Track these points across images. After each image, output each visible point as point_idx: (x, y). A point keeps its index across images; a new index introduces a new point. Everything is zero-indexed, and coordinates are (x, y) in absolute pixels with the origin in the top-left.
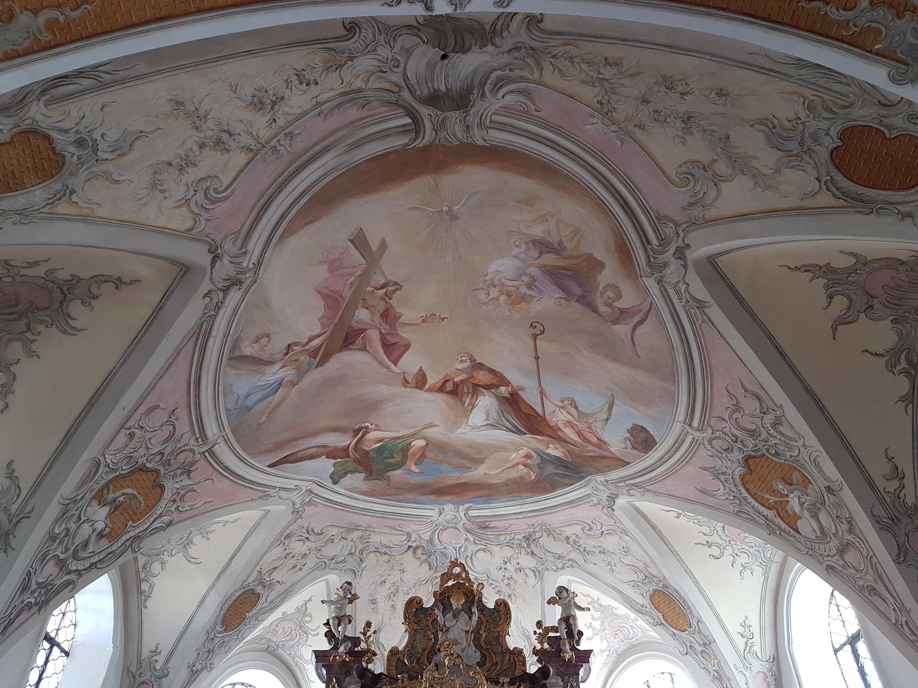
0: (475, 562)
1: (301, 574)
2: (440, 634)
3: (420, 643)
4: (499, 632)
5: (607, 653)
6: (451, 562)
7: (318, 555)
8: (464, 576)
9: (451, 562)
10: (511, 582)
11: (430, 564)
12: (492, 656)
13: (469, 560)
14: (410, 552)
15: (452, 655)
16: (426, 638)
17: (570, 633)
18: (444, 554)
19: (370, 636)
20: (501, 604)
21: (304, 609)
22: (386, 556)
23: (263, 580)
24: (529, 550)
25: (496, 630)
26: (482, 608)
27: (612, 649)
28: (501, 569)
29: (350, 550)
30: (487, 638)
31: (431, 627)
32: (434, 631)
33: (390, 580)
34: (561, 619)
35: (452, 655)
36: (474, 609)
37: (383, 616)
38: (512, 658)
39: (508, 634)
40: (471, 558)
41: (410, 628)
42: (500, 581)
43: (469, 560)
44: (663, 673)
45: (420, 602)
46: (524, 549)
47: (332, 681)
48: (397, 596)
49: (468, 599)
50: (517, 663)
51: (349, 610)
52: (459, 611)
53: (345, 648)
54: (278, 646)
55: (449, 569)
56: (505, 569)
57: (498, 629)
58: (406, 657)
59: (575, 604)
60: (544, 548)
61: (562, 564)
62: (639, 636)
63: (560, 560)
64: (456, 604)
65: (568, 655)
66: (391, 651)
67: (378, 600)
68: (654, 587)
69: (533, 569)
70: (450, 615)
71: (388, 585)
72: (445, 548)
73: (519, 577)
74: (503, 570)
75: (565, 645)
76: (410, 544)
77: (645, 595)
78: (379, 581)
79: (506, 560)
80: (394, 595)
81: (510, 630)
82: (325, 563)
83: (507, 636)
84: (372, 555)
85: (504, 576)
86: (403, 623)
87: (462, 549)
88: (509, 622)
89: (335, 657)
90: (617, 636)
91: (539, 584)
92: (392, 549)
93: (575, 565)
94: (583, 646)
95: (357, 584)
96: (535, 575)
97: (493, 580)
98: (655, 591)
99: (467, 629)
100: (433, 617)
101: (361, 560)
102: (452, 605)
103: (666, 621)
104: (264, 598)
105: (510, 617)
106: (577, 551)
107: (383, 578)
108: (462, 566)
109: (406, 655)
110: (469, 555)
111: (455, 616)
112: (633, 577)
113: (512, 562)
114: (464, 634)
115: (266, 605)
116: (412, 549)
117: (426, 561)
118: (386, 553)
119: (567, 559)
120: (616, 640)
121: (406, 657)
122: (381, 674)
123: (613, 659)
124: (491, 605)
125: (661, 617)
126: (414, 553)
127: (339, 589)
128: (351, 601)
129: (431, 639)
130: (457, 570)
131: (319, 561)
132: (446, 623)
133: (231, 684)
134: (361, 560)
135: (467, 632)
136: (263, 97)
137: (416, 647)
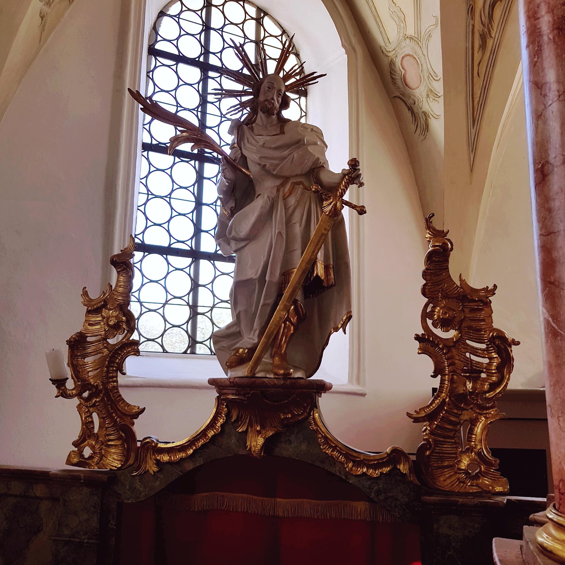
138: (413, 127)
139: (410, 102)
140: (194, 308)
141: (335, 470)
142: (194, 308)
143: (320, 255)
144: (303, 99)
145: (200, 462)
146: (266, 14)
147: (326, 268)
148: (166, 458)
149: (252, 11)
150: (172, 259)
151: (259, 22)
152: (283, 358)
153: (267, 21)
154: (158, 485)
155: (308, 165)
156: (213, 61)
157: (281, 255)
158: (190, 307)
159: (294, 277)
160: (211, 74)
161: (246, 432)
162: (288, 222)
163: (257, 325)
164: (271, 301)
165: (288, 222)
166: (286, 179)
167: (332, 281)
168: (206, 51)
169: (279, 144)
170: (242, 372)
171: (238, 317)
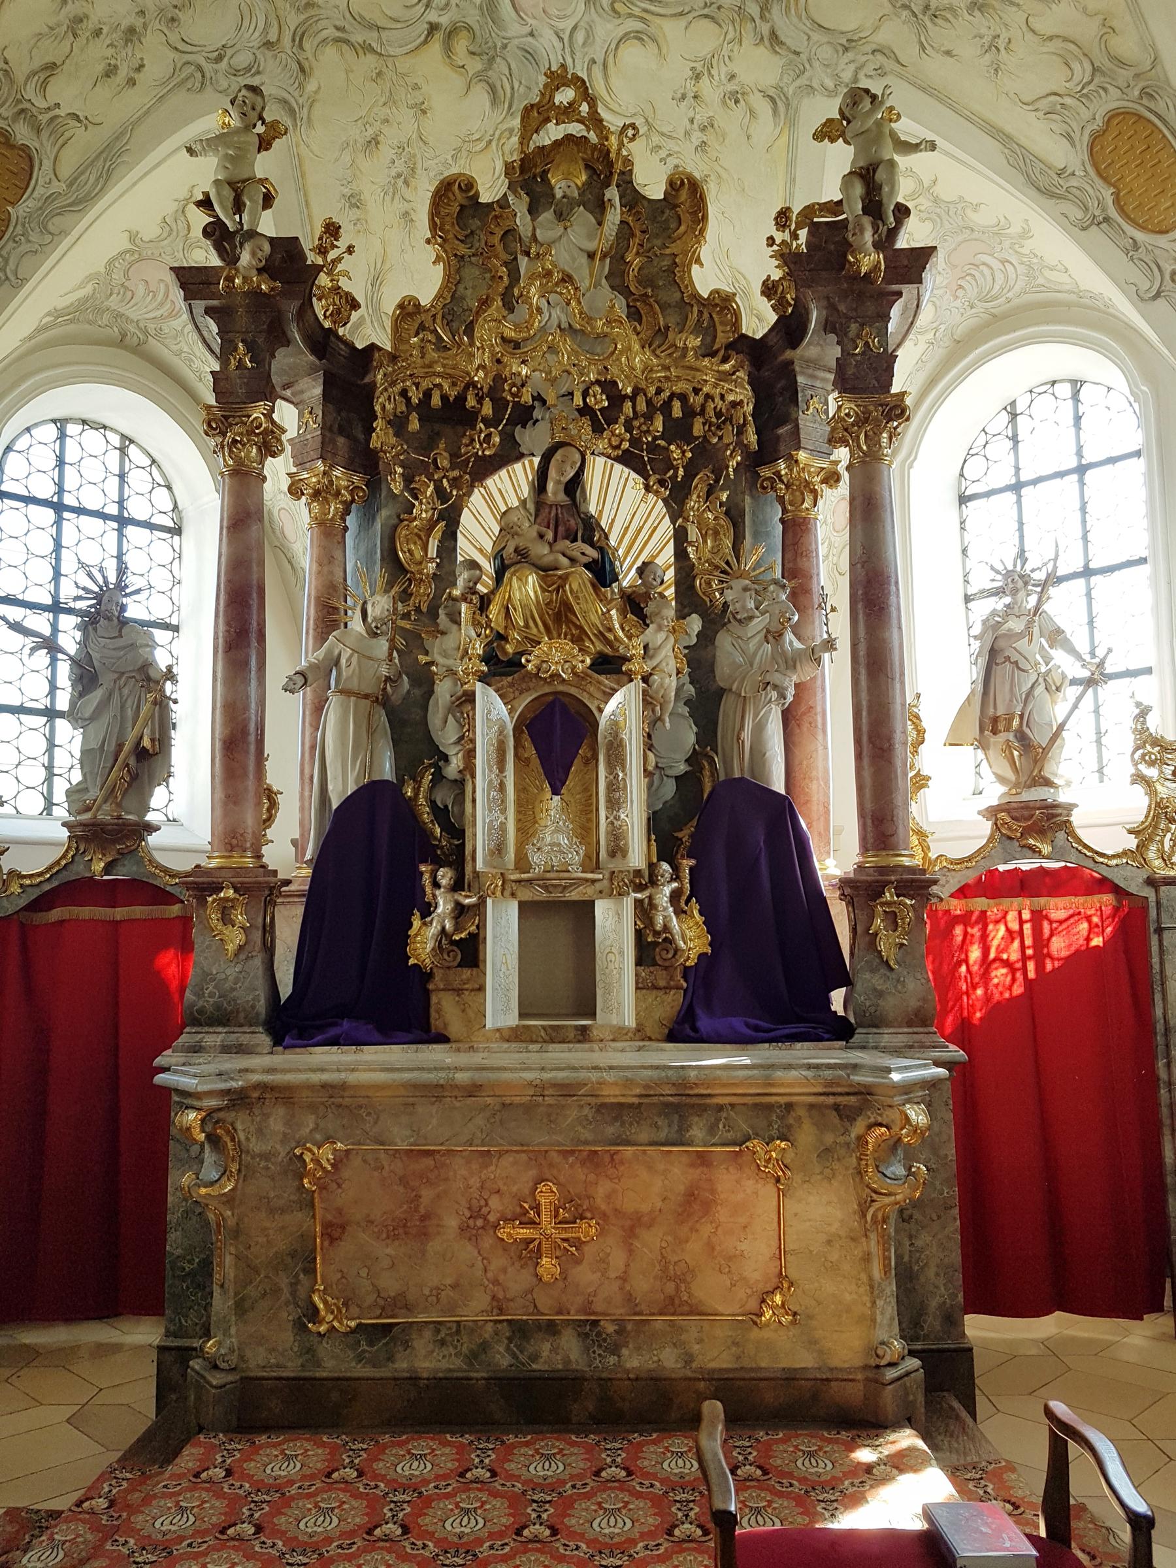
0: (614, 81)
1: (136, 99)
2: (523, 262)
3: (474, 287)
4: (676, 256)
5: (930, 335)
6: (550, 74)
7: (174, 38)
8: (584, 108)
9: (550, 74)
10: (709, 137)
11: (493, 89)
12: (655, 313)
13: (597, 71)
14: (436, 46)
15: (549, 274)
16: (488, 275)
17: (873, 207)
18: (530, 55)
19: (339, 260)
20: (682, 183)
21: (181, 225)
22: (371, 59)
23: (28, 105)
24: (765, 29)
25: (668, 251)
26: (633, 198)
27: (943, 327)
28: (683, 97)
29: (265, 31)
30: (646, 271)
31: (500, 248)
32: (506, 257)
33: (391, 137)
34: (851, 173)
35: (549, 274)
36: (612, 193)
37: (383, 242)
38: (706, 315)
39: (698, 261)
40: (605, 66)
41: (445, 251)
42: (681, 135)
43: (597, 71)
44: (1054, 383)
45: (468, 185)
46: (750, 26)
47: (236, 349)
48: (413, 182)
49: (595, 177)
50: (719, 328)
51: (264, 165)
52: (572, 203)
53: (253, 254)
54: (145, 331)
55: (543, 94)
56: (695, 97)
57: (674, 248)
58: (439, 320)
59: (893, 134)
60: (809, 17)
61: (852, 67)
62: (1017, 288)
63: (850, 55)
64: (563, 184)
65: (868, 260)
66: (401, 306)
67: (366, 196)
68: (1113, 101)
69: (771, 92)
70: (547, 216)
71: (386, 152)
72: (532, 34)
73: (731, 120)
74: (689, 100)
75: (862, 230)
76: (433, 16)
77: (1076, 136)
78: (361, 141)
79: (699, 66)
80: (406, 183)
81: (705, 252)
82: (200, 68)
83: (695, 268)
84: (330, 52)
85: (692, 121)
86: (428, 242)
87: (580, 37)
88: (702, 231)
89: (230, 279)
90: (960, 293)
91: (784, 139)
92: (384, 34)
93: (890, 65)
94: (910, 237)
95: (303, 146)
96: (775, 111)
97: (663, 134)
98: (1113, 116)
99: (591, 246)
100: (506, 224)
101: (302, 70)
102: (552, 188)
103: (1122, 210)
104: (47, 164)
105: (705, 218)
106: (905, 13)
107: (371, 131)
108: (581, 85)
109: (439, 317)
110: (600, 59)
111: (560, 216)
112: (1057, 79)
113: (713, 72)
114: (584, 260)
115: (58, 187)
116: (438, 36)
117: (481, 77)
118: (368, 49)
119: (868, 48)
120: (958, 303)
121: (439, 320)
122: (373, 347)
123: (940, 352)
124: (655, 190)
125: (1109, 200)
126: (448, 49)
127: (229, 107)
128: (264, 144)
129: (501, 277)
130: (565, 96)
131: (181, 59)
132: (538, 232)
133: (54, 421)
134: (302, 70)
135: (591, 256)
136: (792, 1284)
137: (463, 298)
138: (293, 580)
139: (289, 555)
140: (49, 768)
141: (156, 883)
142: (49, 768)
143: (147, 731)
144: (176, 538)
145: (55, 883)
146: (132, 441)
147: (153, 740)
148: (28, 882)
149: (115, 440)
150: (24, 718)
151: (123, 450)
152: (119, 805)
153: (133, 450)
154: (23, 903)
155: (140, 663)
156: (69, 500)
157: (116, 730)
158: (46, 768)
159: (127, 747)
160: (66, 515)
161: (91, 860)
162: (123, 707)
163: (98, 783)
164: (109, 765)
165: (123, 707)
166: (123, 673)
167: (157, 750)
168: (61, 490)
169: (116, 646)
170: (86, 817)
171: (84, 775)
